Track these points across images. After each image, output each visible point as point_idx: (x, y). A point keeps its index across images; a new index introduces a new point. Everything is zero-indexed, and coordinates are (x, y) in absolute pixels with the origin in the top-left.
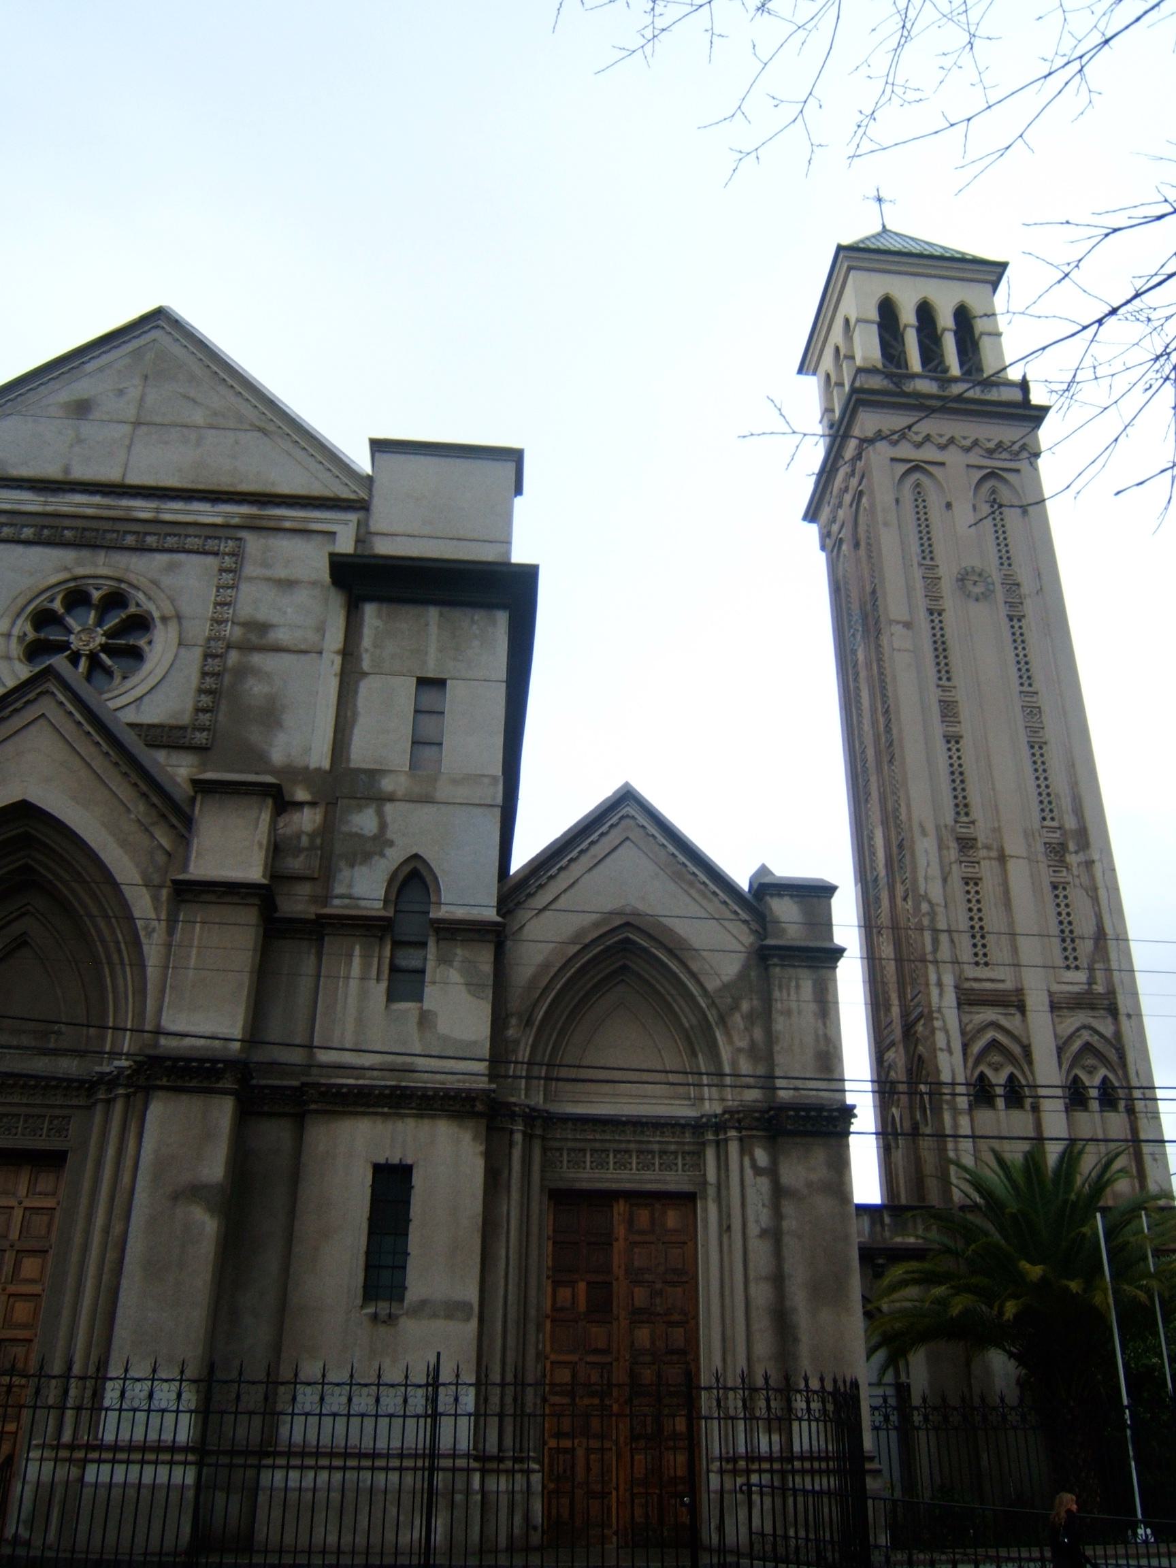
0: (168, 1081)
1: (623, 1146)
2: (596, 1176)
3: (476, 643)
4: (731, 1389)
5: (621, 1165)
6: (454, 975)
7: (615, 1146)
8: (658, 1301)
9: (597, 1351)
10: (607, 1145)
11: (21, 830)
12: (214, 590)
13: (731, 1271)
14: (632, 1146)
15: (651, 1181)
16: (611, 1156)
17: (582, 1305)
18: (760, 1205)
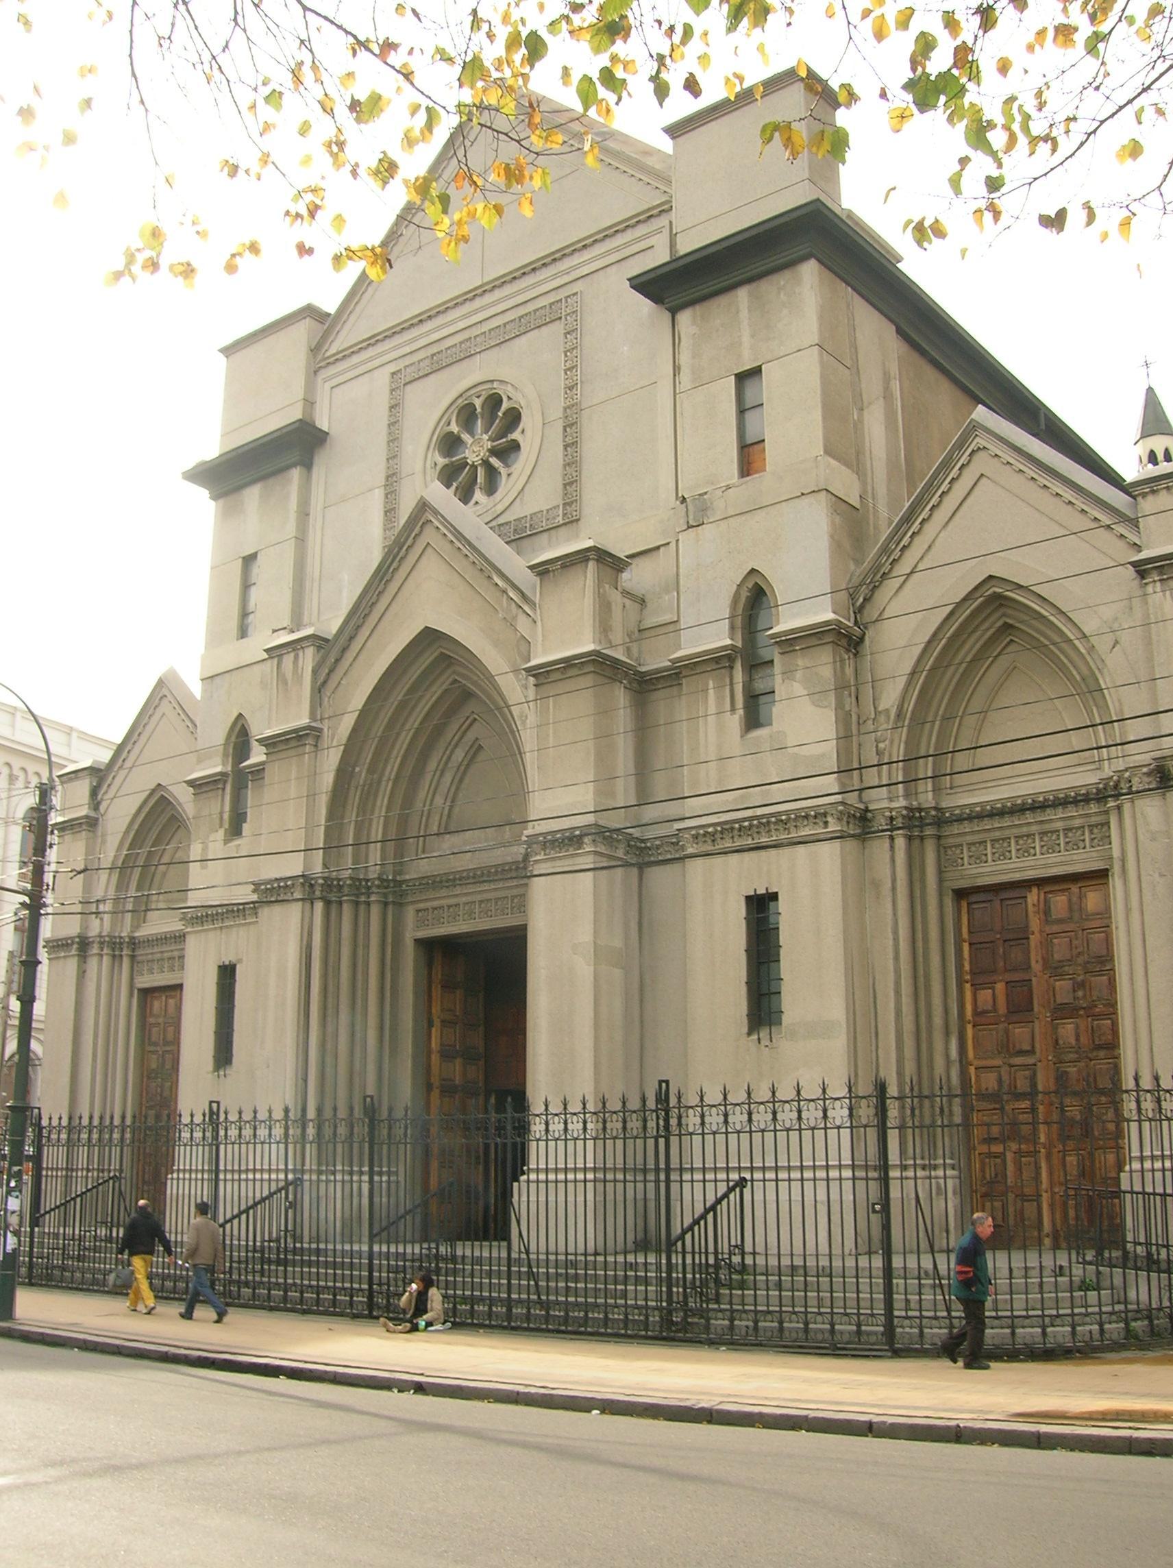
0: (545, 855)
1: (1025, 830)
2: (998, 868)
3: (785, 311)
4: (926, 1097)
5: (1026, 852)
6: (798, 688)
7: (1016, 831)
8: (1080, 994)
9: (1021, 1053)
10: (1007, 833)
11: (436, 654)
12: (563, 355)
13: (381, 1028)
14: (1034, 828)
15: (1056, 865)
16: (1013, 841)
17: (1002, 1008)
18: (1156, 875)
